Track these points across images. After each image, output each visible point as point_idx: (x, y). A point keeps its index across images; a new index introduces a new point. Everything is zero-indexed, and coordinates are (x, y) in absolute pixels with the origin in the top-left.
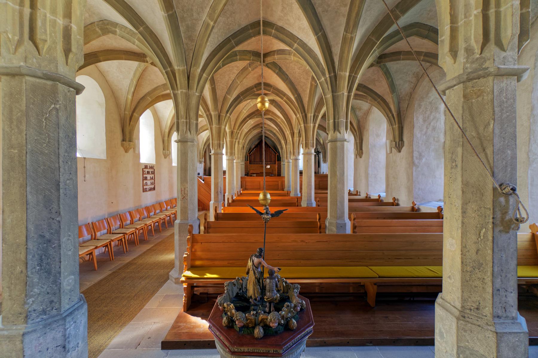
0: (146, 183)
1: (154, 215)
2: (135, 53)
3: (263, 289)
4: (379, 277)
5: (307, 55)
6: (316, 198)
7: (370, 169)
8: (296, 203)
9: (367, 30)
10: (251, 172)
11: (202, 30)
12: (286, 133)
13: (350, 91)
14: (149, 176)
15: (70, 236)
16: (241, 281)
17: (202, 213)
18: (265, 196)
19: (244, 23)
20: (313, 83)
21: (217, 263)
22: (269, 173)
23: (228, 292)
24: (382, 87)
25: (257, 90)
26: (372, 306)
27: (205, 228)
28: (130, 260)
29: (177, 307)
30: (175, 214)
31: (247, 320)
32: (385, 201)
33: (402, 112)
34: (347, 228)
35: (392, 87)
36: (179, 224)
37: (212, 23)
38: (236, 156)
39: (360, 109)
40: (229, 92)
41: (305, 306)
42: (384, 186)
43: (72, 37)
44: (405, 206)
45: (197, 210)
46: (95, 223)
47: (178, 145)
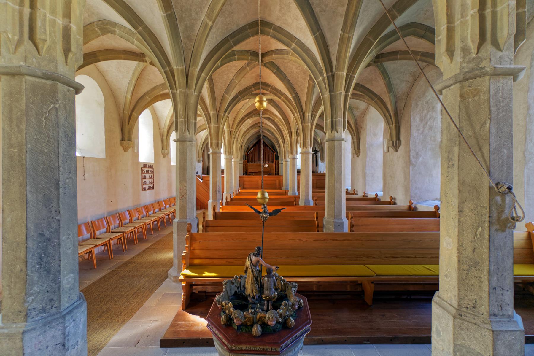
0: (145, 182)
1: (153, 213)
2: (134, 53)
3: (261, 287)
4: (376, 276)
5: (304, 54)
6: (313, 197)
7: (367, 168)
8: (294, 201)
9: (364, 30)
10: (249, 171)
11: (200, 30)
12: (284, 133)
13: (347, 91)
14: (148, 175)
15: (69, 234)
16: (239, 280)
17: (201, 212)
18: (263, 194)
19: (242, 23)
20: (311, 82)
21: (215, 261)
22: (267, 172)
23: (226, 290)
24: (379, 87)
25: (256, 90)
26: (369, 304)
27: (203, 226)
28: (129, 258)
29: (175, 306)
30: (174, 213)
31: (245, 318)
32: (382, 200)
33: (399, 111)
34: (344, 226)
35: (389, 86)
36: (178, 222)
37: (210, 23)
38: (235, 155)
39: (357, 108)
40: (227, 91)
41: (303, 304)
42: (381, 185)
43: (72, 36)
44: (402, 205)
45: (195, 209)
46: (94, 222)
47: (176, 144)
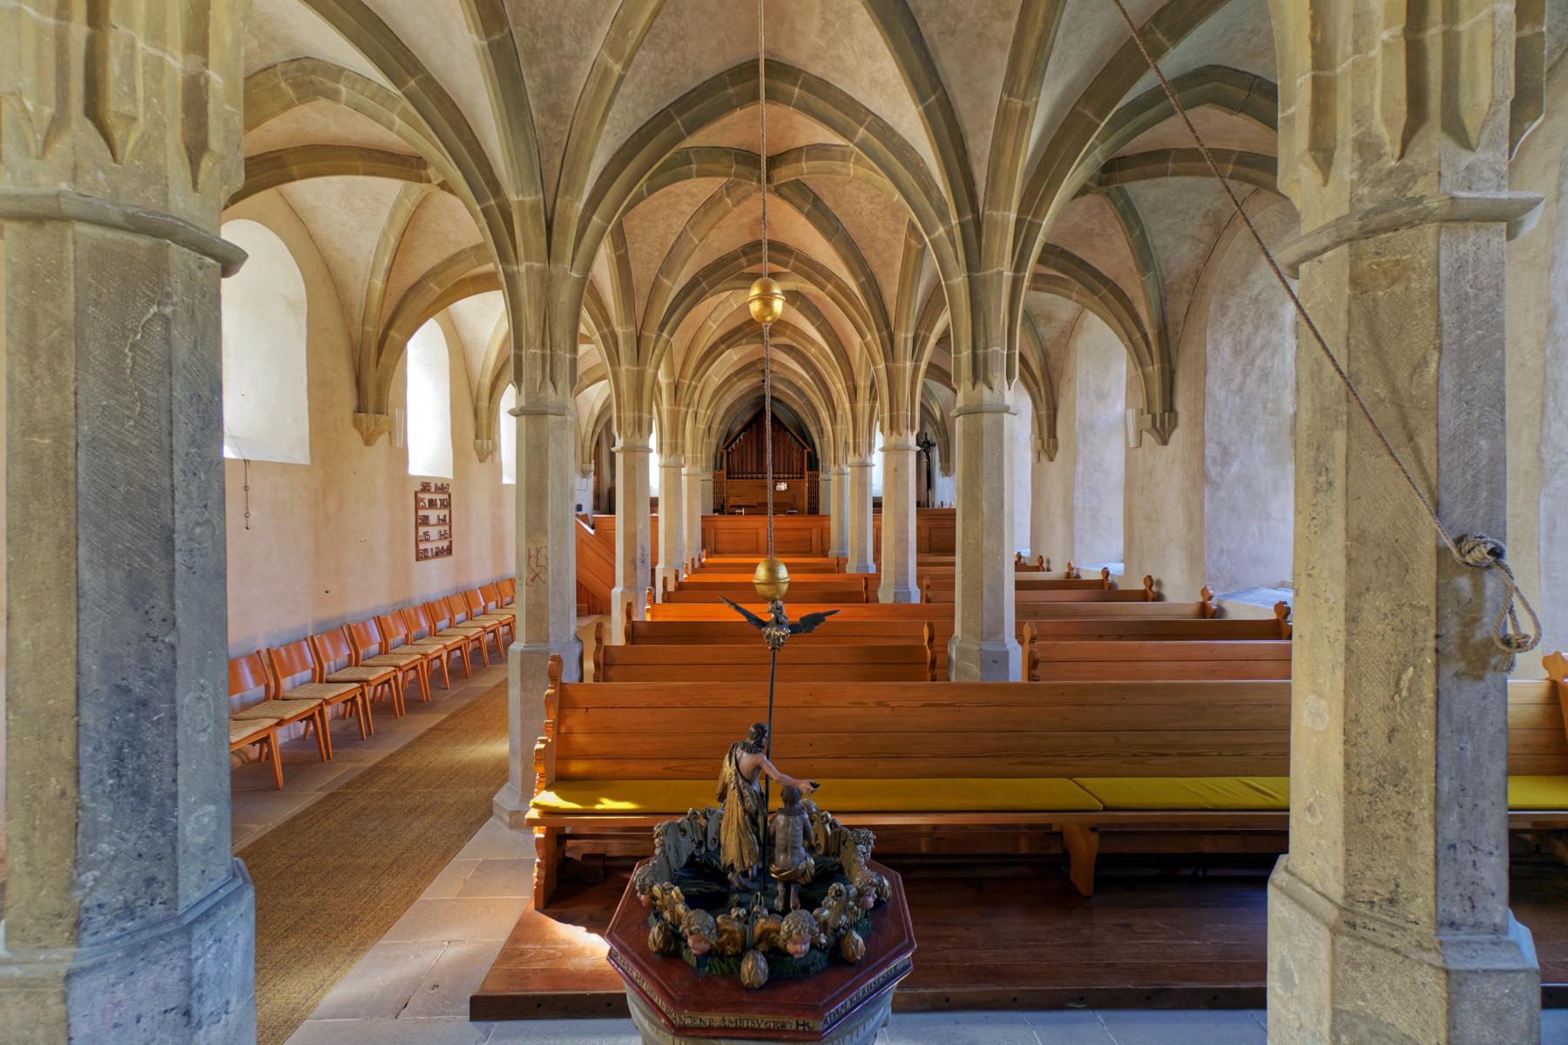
0: (426, 533)
1: (450, 627)
2: (393, 154)
3: (767, 844)
4: (1105, 809)
5: (894, 159)
6: (920, 578)
7: (1078, 494)
8: (863, 591)
9: (1070, 88)
10: (732, 501)
11: (588, 88)
12: (833, 390)
13: (1019, 266)
14: (433, 515)
15: (203, 688)
16: (702, 822)
17: (590, 621)
18: (772, 571)
19: (712, 67)
20: (913, 242)
21: (632, 767)
22: (784, 506)
23: (663, 851)
24: (1112, 255)
25: (750, 263)
26: (1084, 892)
27: (597, 665)
28: (380, 758)
29: (515, 897)
30: (510, 625)
31: (720, 933)
32: (1121, 587)
33: (1170, 327)
34: (1011, 664)
35: (1144, 253)
36: (522, 652)
37: (617, 68)
38: (689, 454)
39: (1049, 318)
40: (667, 267)
41: (889, 893)
42: (1119, 544)
43: (211, 107)
44: (1181, 601)
45: (573, 612)
46: (277, 651)
47: (518, 423)
